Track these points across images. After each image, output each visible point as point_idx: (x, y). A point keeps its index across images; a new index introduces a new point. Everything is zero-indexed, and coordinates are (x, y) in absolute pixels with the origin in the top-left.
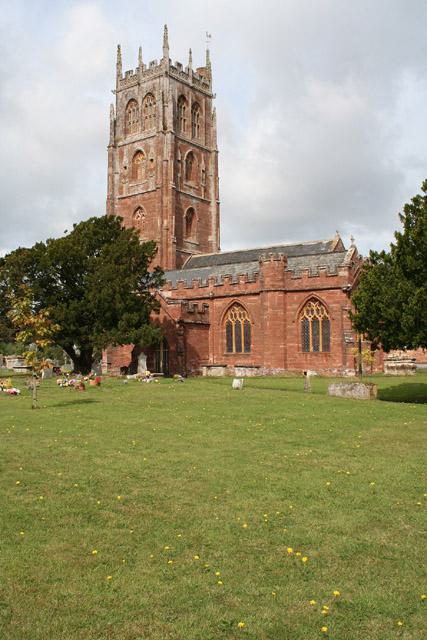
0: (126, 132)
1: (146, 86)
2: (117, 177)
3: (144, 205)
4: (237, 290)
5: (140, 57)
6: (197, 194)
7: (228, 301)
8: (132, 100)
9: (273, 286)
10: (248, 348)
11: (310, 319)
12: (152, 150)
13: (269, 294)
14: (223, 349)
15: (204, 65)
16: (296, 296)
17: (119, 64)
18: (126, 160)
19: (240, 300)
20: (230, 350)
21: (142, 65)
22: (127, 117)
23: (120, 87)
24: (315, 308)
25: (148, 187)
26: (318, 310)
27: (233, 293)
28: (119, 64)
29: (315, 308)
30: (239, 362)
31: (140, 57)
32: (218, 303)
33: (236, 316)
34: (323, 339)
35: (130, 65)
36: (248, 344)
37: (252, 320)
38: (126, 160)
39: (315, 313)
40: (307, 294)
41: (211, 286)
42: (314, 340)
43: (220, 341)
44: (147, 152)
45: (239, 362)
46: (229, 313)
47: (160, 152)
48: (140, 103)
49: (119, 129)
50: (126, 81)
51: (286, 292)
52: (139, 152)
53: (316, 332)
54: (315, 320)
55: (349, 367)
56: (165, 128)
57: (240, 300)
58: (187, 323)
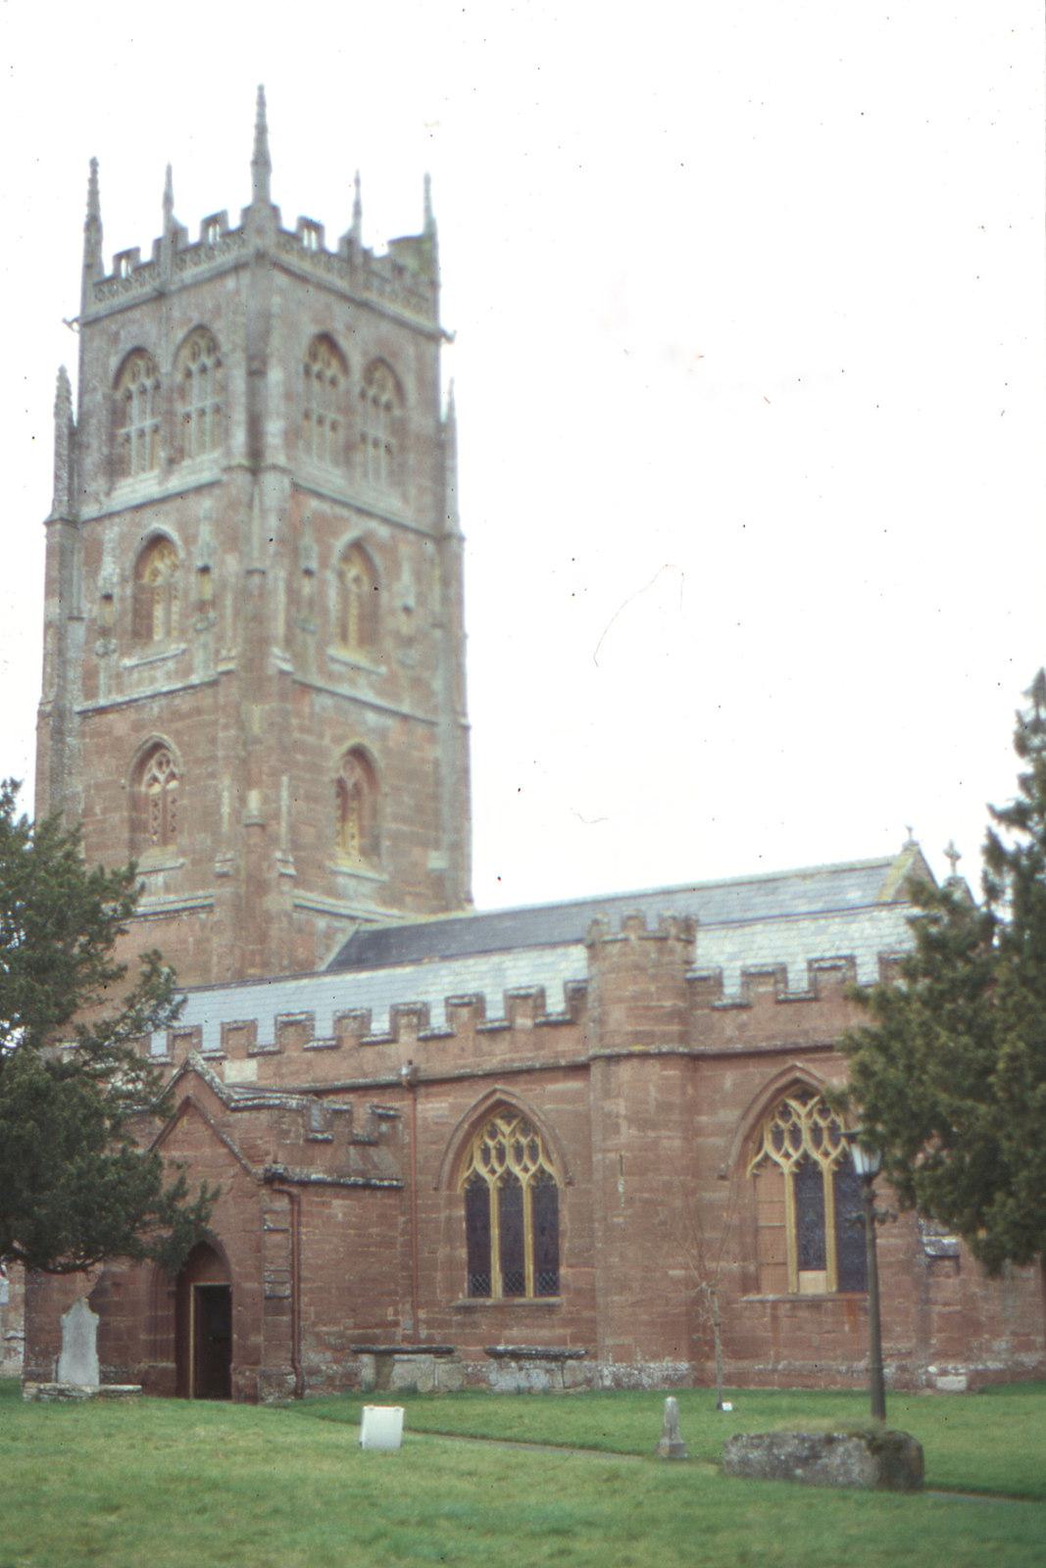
0: (115, 468)
1: (184, 311)
2: (78, 632)
3: (177, 734)
4: (499, 1055)
5: (168, 201)
7: (470, 1098)
8: (138, 351)
9: (638, 1037)
10: (548, 1283)
12: (205, 532)
13: (625, 1072)
14: (452, 1288)
15: (416, 229)
16: (729, 1078)
17: (93, 224)
18: (110, 569)
20: (481, 1287)
21: (175, 232)
22: (118, 415)
23: (100, 308)
25: (188, 671)
26: (816, 1131)
27: (492, 1063)
28: (93, 224)
29: (804, 1125)
30: (516, 1336)
31: (168, 201)
32: (435, 1108)
33: (501, 1157)
34: (538, 1270)
35: (133, 229)
36: (548, 1263)
37: (565, 1170)
38: (110, 569)
39: (510, 1161)
41: (406, 1038)
43: (442, 1252)
44: (189, 540)
45: (516, 1336)
46: (476, 1143)
47: (233, 538)
48: (165, 367)
49: (92, 459)
51: (696, 1058)
52: (158, 541)
53: (811, 1216)
56: (256, 451)
57: (519, 1094)
58: (304, 1184)
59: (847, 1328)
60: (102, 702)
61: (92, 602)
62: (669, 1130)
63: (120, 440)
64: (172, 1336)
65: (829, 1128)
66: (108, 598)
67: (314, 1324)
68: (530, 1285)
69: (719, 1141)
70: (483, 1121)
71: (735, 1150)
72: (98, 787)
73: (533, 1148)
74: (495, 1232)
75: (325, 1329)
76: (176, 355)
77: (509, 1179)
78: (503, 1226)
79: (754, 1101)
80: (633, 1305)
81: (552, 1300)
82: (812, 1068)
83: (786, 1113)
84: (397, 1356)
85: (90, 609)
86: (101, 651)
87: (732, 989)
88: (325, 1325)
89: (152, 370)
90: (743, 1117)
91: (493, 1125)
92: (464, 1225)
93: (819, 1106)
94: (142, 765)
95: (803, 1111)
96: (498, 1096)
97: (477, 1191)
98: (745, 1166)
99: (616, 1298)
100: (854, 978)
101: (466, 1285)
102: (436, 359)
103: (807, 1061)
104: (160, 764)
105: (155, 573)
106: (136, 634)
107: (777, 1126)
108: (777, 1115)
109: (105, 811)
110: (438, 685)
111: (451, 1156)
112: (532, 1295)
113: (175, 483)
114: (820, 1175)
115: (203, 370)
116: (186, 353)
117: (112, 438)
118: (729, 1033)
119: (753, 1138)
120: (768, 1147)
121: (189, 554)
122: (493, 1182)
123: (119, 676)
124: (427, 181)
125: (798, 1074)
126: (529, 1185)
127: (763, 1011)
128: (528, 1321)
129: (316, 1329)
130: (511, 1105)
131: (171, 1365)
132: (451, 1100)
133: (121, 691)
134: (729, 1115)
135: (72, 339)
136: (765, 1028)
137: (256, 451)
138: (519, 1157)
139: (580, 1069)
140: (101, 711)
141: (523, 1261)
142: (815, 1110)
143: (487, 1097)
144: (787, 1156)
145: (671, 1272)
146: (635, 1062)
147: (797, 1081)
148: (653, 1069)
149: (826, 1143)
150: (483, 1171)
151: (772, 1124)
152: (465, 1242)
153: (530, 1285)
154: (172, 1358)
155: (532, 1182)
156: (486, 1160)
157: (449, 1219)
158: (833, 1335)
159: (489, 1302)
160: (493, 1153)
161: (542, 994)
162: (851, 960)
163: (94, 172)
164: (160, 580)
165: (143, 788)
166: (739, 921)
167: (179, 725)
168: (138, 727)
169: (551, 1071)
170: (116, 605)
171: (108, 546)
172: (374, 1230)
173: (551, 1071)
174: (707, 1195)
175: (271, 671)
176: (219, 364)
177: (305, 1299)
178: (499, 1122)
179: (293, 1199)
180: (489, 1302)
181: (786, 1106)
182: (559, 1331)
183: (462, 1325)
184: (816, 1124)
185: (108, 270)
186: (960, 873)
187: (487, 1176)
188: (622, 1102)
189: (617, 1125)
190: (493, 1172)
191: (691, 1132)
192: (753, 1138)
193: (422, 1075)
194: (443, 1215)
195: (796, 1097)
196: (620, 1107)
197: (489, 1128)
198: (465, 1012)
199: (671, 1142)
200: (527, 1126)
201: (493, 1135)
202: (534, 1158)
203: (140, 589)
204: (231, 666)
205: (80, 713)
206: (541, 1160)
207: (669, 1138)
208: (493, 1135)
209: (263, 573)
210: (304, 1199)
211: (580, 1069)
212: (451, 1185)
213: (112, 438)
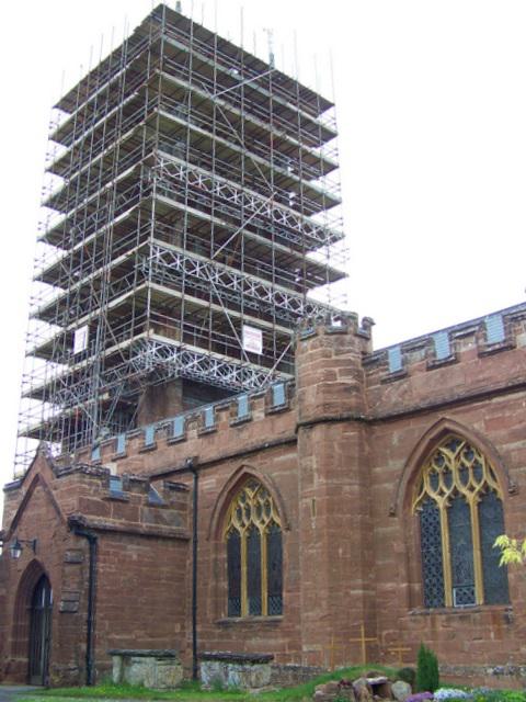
7: (226, 472)
10: (276, 605)
11: (441, 502)
14: (217, 610)
16: (396, 435)
19: (459, 420)
20: (235, 609)
26: (463, 470)
29: (453, 467)
32: (210, 483)
33: (248, 515)
36: (276, 589)
40: (424, 424)
46: (233, 506)
54: (457, 502)
59: (492, 635)
62: (351, 478)
64: (27, 639)
65: (473, 467)
67: (108, 633)
69: (389, 486)
73: (267, 505)
74: (244, 569)
75: (118, 637)
77: (253, 529)
78: (249, 564)
79: (415, 450)
80: (322, 619)
81: (279, 617)
82: (457, 418)
83: (440, 459)
84: (133, 659)
87: (395, 364)
88: (117, 634)
90: (406, 465)
91: (244, 493)
92: (226, 565)
93: (465, 450)
95: (452, 456)
98: (410, 505)
99: (310, 614)
100: (434, 355)
101: (226, 608)
103: (453, 414)
107: (434, 471)
108: (433, 461)
111: (216, 515)
112: (266, 614)
118: (393, 398)
119: (414, 480)
120: (427, 488)
122: (243, 533)
125: (447, 425)
126: (265, 533)
128: (260, 634)
129: (110, 637)
130: (255, 477)
131: (25, 660)
132: (217, 476)
134: (396, 464)
136: (422, 388)
141: (260, 590)
142: (462, 454)
143: (237, 472)
144: (442, 493)
145: (352, 592)
146: (324, 426)
147: (446, 431)
148: (337, 429)
150: (237, 525)
151: (429, 470)
152: (226, 577)
153: (363, 635)
154: (26, 654)
155: (267, 531)
157: (216, 560)
158: (481, 641)
159: (238, 619)
160: (244, 512)
166: (414, 349)
172: (165, 569)
174: (381, 530)
177: (99, 615)
178: (248, 490)
179: (92, 541)
180: (238, 619)
181: (440, 453)
182: (281, 641)
183: (221, 636)
184: (463, 465)
187: (239, 529)
188: (313, 458)
189: (312, 476)
191: (367, 479)
192: (414, 480)
194: (213, 556)
195: (447, 446)
196: (313, 462)
197: (241, 494)
199: (351, 487)
200: (263, 491)
206: (272, 514)
207: (350, 484)
208: (243, 500)
210: (99, 542)
212: (217, 536)
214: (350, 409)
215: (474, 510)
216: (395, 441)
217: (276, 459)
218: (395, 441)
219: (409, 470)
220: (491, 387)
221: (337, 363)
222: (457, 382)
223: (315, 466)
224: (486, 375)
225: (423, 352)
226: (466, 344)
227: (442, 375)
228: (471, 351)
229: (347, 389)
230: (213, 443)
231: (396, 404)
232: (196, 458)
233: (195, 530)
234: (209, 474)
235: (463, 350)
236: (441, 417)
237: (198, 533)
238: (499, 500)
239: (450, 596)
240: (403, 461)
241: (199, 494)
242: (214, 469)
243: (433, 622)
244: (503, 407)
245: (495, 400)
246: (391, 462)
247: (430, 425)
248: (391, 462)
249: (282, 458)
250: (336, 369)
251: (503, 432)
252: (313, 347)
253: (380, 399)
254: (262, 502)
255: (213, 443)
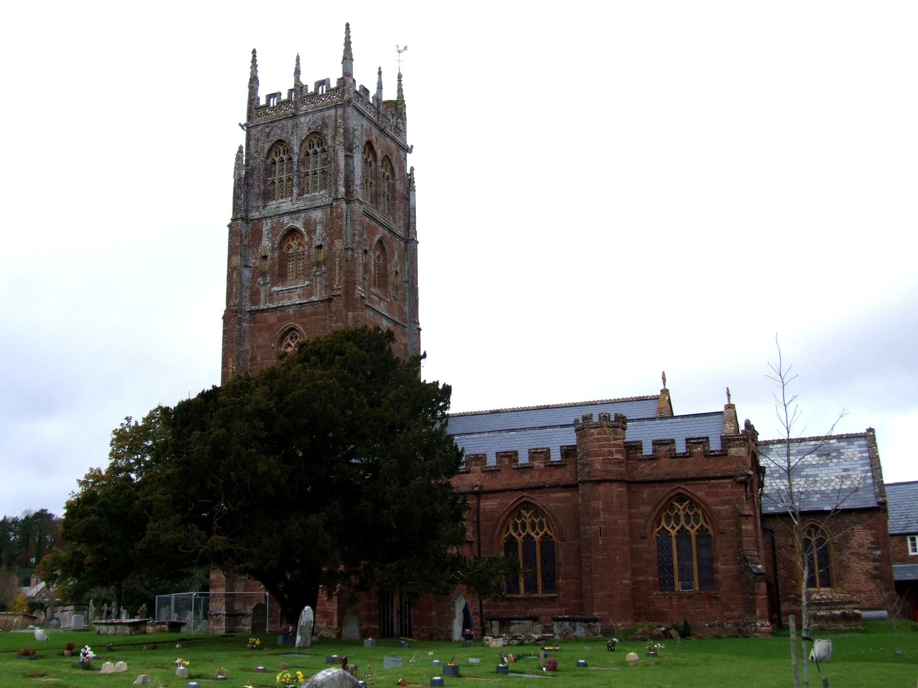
0: (267, 196)
3: (304, 324)
4: (527, 479)
5: (297, 72)
6: (389, 311)
7: (511, 500)
8: (280, 142)
11: (673, 533)
16: (646, 493)
17: (254, 82)
19: (689, 489)
22: (269, 171)
24: (681, 513)
25: (311, 294)
26: (687, 516)
28: (254, 82)
29: (528, 521)
31: (297, 72)
32: (488, 504)
33: (524, 527)
35: (276, 82)
39: (528, 530)
40: (667, 489)
42: (681, 570)
50: (259, 115)
52: (293, 232)
54: (683, 534)
55: (761, 618)
56: (348, 192)
57: (537, 499)
60: (262, 307)
61: (256, 259)
63: (269, 183)
66: (265, 257)
68: (540, 588)
69: (641, 521)
70: (515, 511)
71: (649, 525)
72: (259, 347)
76: (301, 144)
78: (544, 562)
79: (661, 500)
83: (672, 508)
85: (252, 261)
86: (262, 283)
87: (647, 450)
89: (288, 151)
90: (654, 510)
94: (283, 338)
96: (524, 499)
97: (511, 544)
100: (675, 450)
102: (405, 159)
104: (292, 338)
105: (289, 247)
106: (279, 275)
109: (262, 359)
110: (406, 309)
111: (499, 527)
113: (300, 205)
114: (690, 536)
115: (316, 153)
116: (306, 144)
117: (265, 181)
118: (644, 471)
120: (663, 523)
121: (311, 239)
123: (271, 295)
124: (400, 76)
125: (681, 491)
127: (664, 462)
133: (272, 302)
135: (243, 134)
136: (666, 468)
137: (348, 192)
138: (533, 529)
139: (574, 487)
140: (263, 311)
148: (614, 486)
149: (537, 529)
153: (540, 588)
156: (516, 529)
161: (516, 453)
162: (673, 442)
163: (254, 56)
164: (291, 251)
165: (283, 349)
166: (663, 444)
167: (304, 320)
168: (280, 320)
169: (556, 487)
170: (269, 262)
171: (265, 232)
173: (556, 487)
175: (357, 296)
176: (324, 151)
181: (672, 504)
185: (263, 102)
186: (732, 403)
190: (520, 535)
193: (485, 488)
195: (677, 501)
198: (506, 460)
201: (519, 518)
202: (541, 529)
203: (282, 254)
204: (339, 293)
205: (250, 312)
206: (546, 529)
209: (352, 250)
211: (574, 487)
213: (265, 181)
214: (621, 474)
215: (693, 539)
216: (645, 495)
217: (552, 495)
218: (645, 495)
219: (654, 514)
220: (712, 475)
221: (614, 446)
222: (690, 468)
223: (601, 507)
224: (709, 467)
225: (668, 448)
226: (696, 448)
227: (680, 463)
228: (700, 452)
229: (619, 462)
230: (496, 477)
231: (648, 475)
232: (481, 486)
233: (479, 536)
234: (491, 498)
235: (695, 450)
236: (677, 486)
237: (482, 538)
238: (710, 535)
239: (678, 586)
240: (651, 507)
241: (482, 511)
242: (496, 495)
243: (670, 599)
244: (718, 486)
245: (712, 481)
246: (642, 507)
247: (669, 490)
248: (642, 507)
249: (558, 495)
250: (613, 450)
251: (716, 500)
252: (598, 434)
253: (636, 469)
254: (537, 521)
255: (496, 477)
